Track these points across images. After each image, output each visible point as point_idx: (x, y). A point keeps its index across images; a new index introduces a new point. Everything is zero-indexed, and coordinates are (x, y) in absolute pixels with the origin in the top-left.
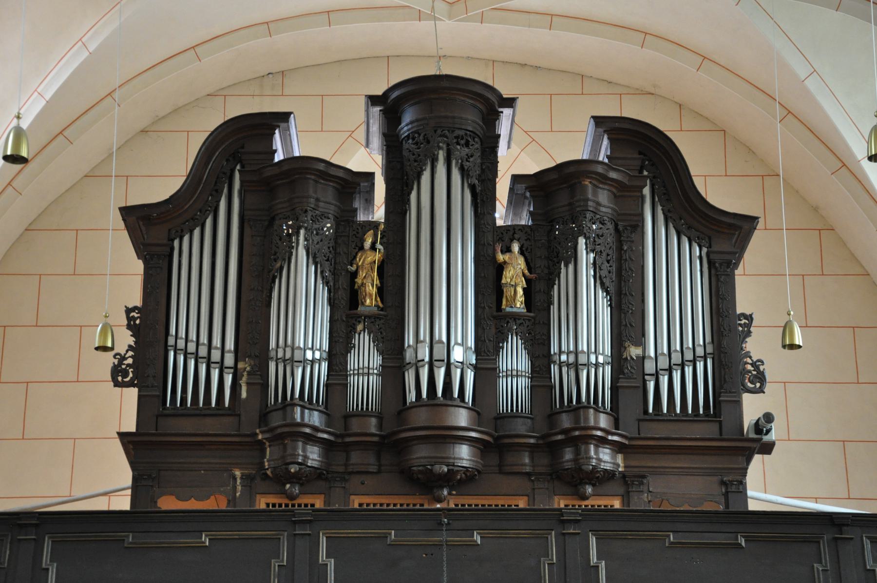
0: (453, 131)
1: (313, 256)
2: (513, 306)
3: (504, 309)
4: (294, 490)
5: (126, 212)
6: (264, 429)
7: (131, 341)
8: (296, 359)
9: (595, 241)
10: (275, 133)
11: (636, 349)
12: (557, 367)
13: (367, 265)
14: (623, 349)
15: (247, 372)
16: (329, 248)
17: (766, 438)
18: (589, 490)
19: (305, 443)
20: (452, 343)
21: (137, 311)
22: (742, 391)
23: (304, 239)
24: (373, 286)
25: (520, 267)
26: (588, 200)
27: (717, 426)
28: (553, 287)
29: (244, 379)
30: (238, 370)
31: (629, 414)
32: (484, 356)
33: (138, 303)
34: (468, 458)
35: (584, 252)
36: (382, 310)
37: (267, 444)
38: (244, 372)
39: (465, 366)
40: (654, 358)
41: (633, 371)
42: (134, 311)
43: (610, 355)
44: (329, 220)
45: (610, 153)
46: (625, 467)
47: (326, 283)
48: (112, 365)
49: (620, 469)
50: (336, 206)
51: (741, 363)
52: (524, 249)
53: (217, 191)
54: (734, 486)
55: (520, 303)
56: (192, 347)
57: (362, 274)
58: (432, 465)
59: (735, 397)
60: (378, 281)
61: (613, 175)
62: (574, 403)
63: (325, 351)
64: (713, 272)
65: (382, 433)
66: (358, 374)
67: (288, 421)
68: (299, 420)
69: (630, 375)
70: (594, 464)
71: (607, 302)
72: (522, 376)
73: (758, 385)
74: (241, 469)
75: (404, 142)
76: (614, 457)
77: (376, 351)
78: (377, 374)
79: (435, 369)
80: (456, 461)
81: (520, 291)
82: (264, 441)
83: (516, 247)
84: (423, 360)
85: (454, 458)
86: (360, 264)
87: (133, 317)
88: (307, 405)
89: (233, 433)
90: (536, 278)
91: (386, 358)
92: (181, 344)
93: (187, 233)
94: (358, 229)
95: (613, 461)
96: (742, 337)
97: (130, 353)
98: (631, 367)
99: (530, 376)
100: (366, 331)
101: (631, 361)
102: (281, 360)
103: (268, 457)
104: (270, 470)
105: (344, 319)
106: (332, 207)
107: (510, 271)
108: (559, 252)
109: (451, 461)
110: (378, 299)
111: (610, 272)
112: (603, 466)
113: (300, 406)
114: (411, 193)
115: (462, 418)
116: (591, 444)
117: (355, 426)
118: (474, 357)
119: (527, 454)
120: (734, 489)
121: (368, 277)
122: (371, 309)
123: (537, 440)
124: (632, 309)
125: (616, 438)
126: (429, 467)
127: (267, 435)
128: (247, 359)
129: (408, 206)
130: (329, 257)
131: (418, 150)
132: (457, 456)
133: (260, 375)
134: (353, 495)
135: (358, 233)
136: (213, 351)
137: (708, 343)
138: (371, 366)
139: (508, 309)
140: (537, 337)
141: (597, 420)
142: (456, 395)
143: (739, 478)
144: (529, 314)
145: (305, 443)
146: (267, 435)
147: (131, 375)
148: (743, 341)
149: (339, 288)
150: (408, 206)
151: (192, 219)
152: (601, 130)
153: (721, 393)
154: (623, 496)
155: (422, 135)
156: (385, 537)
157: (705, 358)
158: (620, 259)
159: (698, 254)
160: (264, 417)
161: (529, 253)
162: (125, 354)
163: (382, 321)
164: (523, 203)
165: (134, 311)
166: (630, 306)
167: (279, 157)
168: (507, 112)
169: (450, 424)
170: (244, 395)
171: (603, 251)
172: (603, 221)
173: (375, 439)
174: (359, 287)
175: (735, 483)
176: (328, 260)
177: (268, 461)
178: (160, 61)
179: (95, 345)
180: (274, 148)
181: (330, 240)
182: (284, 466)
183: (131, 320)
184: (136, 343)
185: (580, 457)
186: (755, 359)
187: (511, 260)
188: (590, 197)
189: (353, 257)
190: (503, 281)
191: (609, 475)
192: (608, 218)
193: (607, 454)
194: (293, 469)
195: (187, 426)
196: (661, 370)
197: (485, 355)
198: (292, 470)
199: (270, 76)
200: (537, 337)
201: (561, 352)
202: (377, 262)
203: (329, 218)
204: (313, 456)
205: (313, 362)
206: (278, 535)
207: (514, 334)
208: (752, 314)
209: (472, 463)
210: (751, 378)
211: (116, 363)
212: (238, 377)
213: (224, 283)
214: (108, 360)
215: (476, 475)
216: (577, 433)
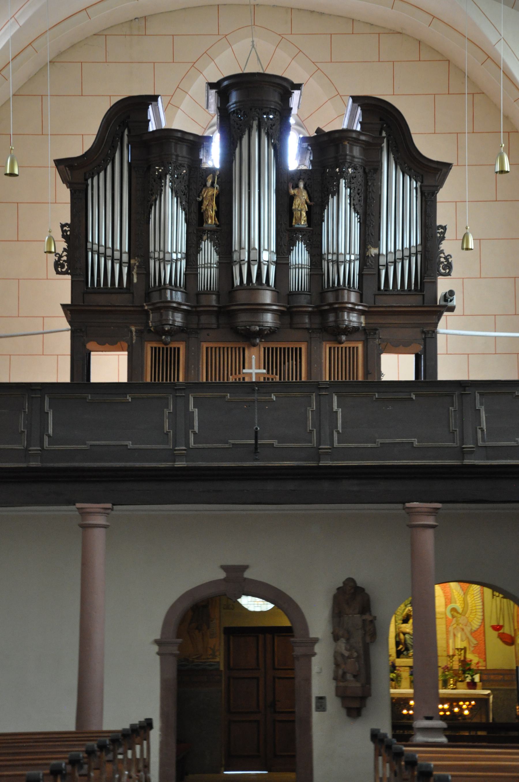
0: (262, 110)
1: (175, 192)
2: (300, 224)
3: (294, 226)
4: (167, 339)
5: (58, 163)
6: (149, 303)
7: (65, 245)
8: (166, 259)
9: (350, 181)
10: (149, 108)
11: (375, 249)
12: (326, 262)
13: (209, 196)
14: (366, 250)
15: (137, 266)
16: (185, 186)
17: (450, 304)
18: (344, 338)
19: (173, 312)
20: (262, 249)
21: (67, 226)
22: (437, 275)
23: (169, 181)
24: (213, 211)
25: (304, 197)
26: (346, 155)
27: (422, 297)
28: (324, 210)
29: (135, 270)
30: (131, 264)
31: (369, 292)
32: (281, 255)
33: (69, 222)
34: (271, 321)
35: (344, 188)
36: (218, 226)
37: (150, 312)
38: (134, 266)
39: (269, 263)
40: (386, 255)
41: (372, 264)
42: (66, 226)
43: (358, 254)
44: (184, 168)
45: (362, 120)
46: (366, 324)
47: (184, 209)
48: (54, 261)
49: (363, 325)
50: (188, 158)
51: (438, 257)
52: (306, 185)
53: (113, 147)
54: (429, 334)
55: (304, 221)
56: (102, 250)
57: (206, 203)
58: (250, 326)
59: (433, 279)
60: (216, 208)
61: (363, 138)
62: (336, 285)
63: (184, 253)
64: (423, 198)
65: (220, 305)
66: (204, 267)
67: (163, 300)
68: (169, 299)
69: (370, 266)
70: (346, 324)
71: (358, 219)
72: (304, 268)
73: (447, 271)
74: (135, 326)
75: (231, 115)
76: (359, 318)
77: (215, 253)
78: (216, 267)
79: (252, 266)
80: (264, 323)
81: (304, 214)
82: (149, 310)
83: (301, 185)
84: (244, 260)
85: (263, 322)
86: (204, 196)
87: (65, 230)
88: (174, 288)
89: (129, 305)
90: (314, 204)
91: (221, 257)
92: (95, 247)
93: (96, 175)
94: (203, 173)
95: (358, 321)
96: (439, 241)
97: (65, 253)
98: (371, 261)
99: (310, 267)
100: (209, 240)
101: (372, 258)
102: (157, 259)
103: (151, 320)
104: (152, 327)
105: (195, 232)
106: (186, 160)
107: (297, 201)
108: (328, 188)
109: (261, 323)
110: (216, 219)
111: (359, 201)
112: (352, 324)
113: (170, 289)
114: (236, 149)
115: (267, 297)
116: (345, 312)
117: (204, 301)
118: (275, 256)
119: (307, 316)
120: (429, 336)
121: (210, 205)
122: (211, 226)
123: (313, 309)
124: (373, 224)
125: (360, 308)
126: (248, 327)
127: (150, 307)
128: (136, 258)
129: (234, 157)
130: (185, 192)
131: (240, 122)
132: (264, 320)
133: (145, 268)
134: (202, 342)
135: (203, 175)
136: (115, 252)
137: (419, 245)
138: (212, 262)
139: (297, 226)
140: (314, 243)
141: (349, 298)
142: (264, 282)
143: (432, 329)
144: (308, 228)
145: (173, 312)
146: (150, 307)
147: (66, 267)
148: (440, 243)
149: (192, 211)
150: (234, 157)
151: (99, 165)
152: (356, 105)
153: (425, 277)
154: (364, 341)
155: (242, 112)
156: (225, 397)
157: (416, 254)
158: (366, 190)
159: (415, 186)
160: (148, 295)
161: (310, 187)
162: (62, 254)
163: (219, 233)
164: (305, 159)
165: (66, 226)
166: (372, 222)
167: (152, 127)
168: (296, 94)
169: (260, 302)
170: (135, 280)
171: (355, 187)
172: (356, 167)
173: (215, 309)
174: (204, 211)
175: (430, 332)
176: (184, 195)
177: (151, 322)
178: (63, 19)
179: (44, 250)
180: (149, 118)
181: (186, 181)
182: (161, 326)
183: (64, 232)
184: (68, 247)
185: (338, 319)
186: (446, 254)
187: (299, 194)
188: (348, 153)
189: (200, 191)
190: (293, 208)
191: (356, 330)
192: (359, 165)
193: (355, 317)
194: (167, 328)
195: (102, 300)
196: (389, 262)
197: (282, 254)
198: (166, 329)
199: (137, 20)
200: (314, 243)
201: (328, 253)
202: (215, 195)
203: (184, 167)
204: (178, 319)
205: (177, 260)
206: (167, 396)
207: (300, 241)
208: (446, 225)
209: (273, 324)
210: (444, 267)
211: (57, 259)
212: (131, 269)
213: (111, 169)
214: (53, 258)
215: (276, 330)
216: (337, 306)
